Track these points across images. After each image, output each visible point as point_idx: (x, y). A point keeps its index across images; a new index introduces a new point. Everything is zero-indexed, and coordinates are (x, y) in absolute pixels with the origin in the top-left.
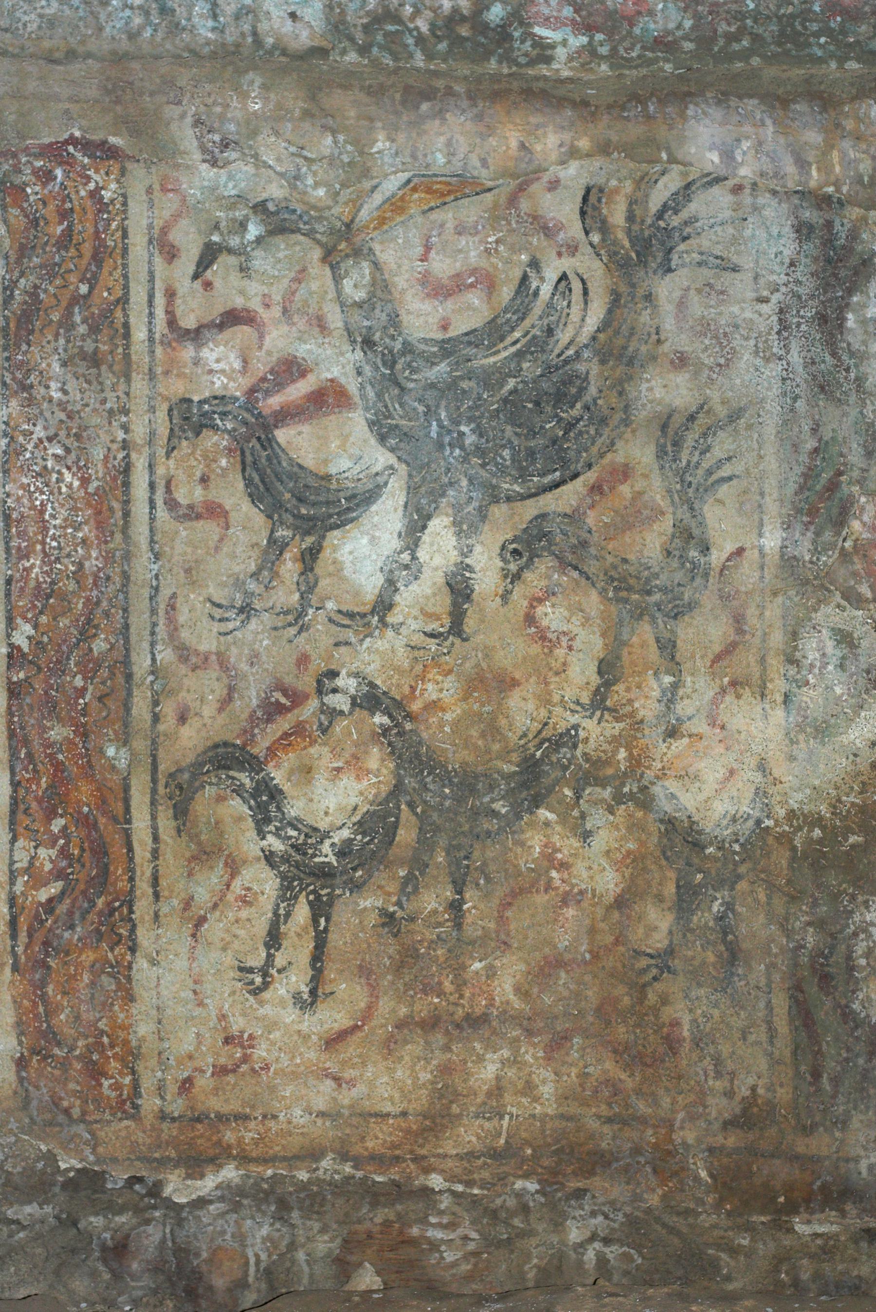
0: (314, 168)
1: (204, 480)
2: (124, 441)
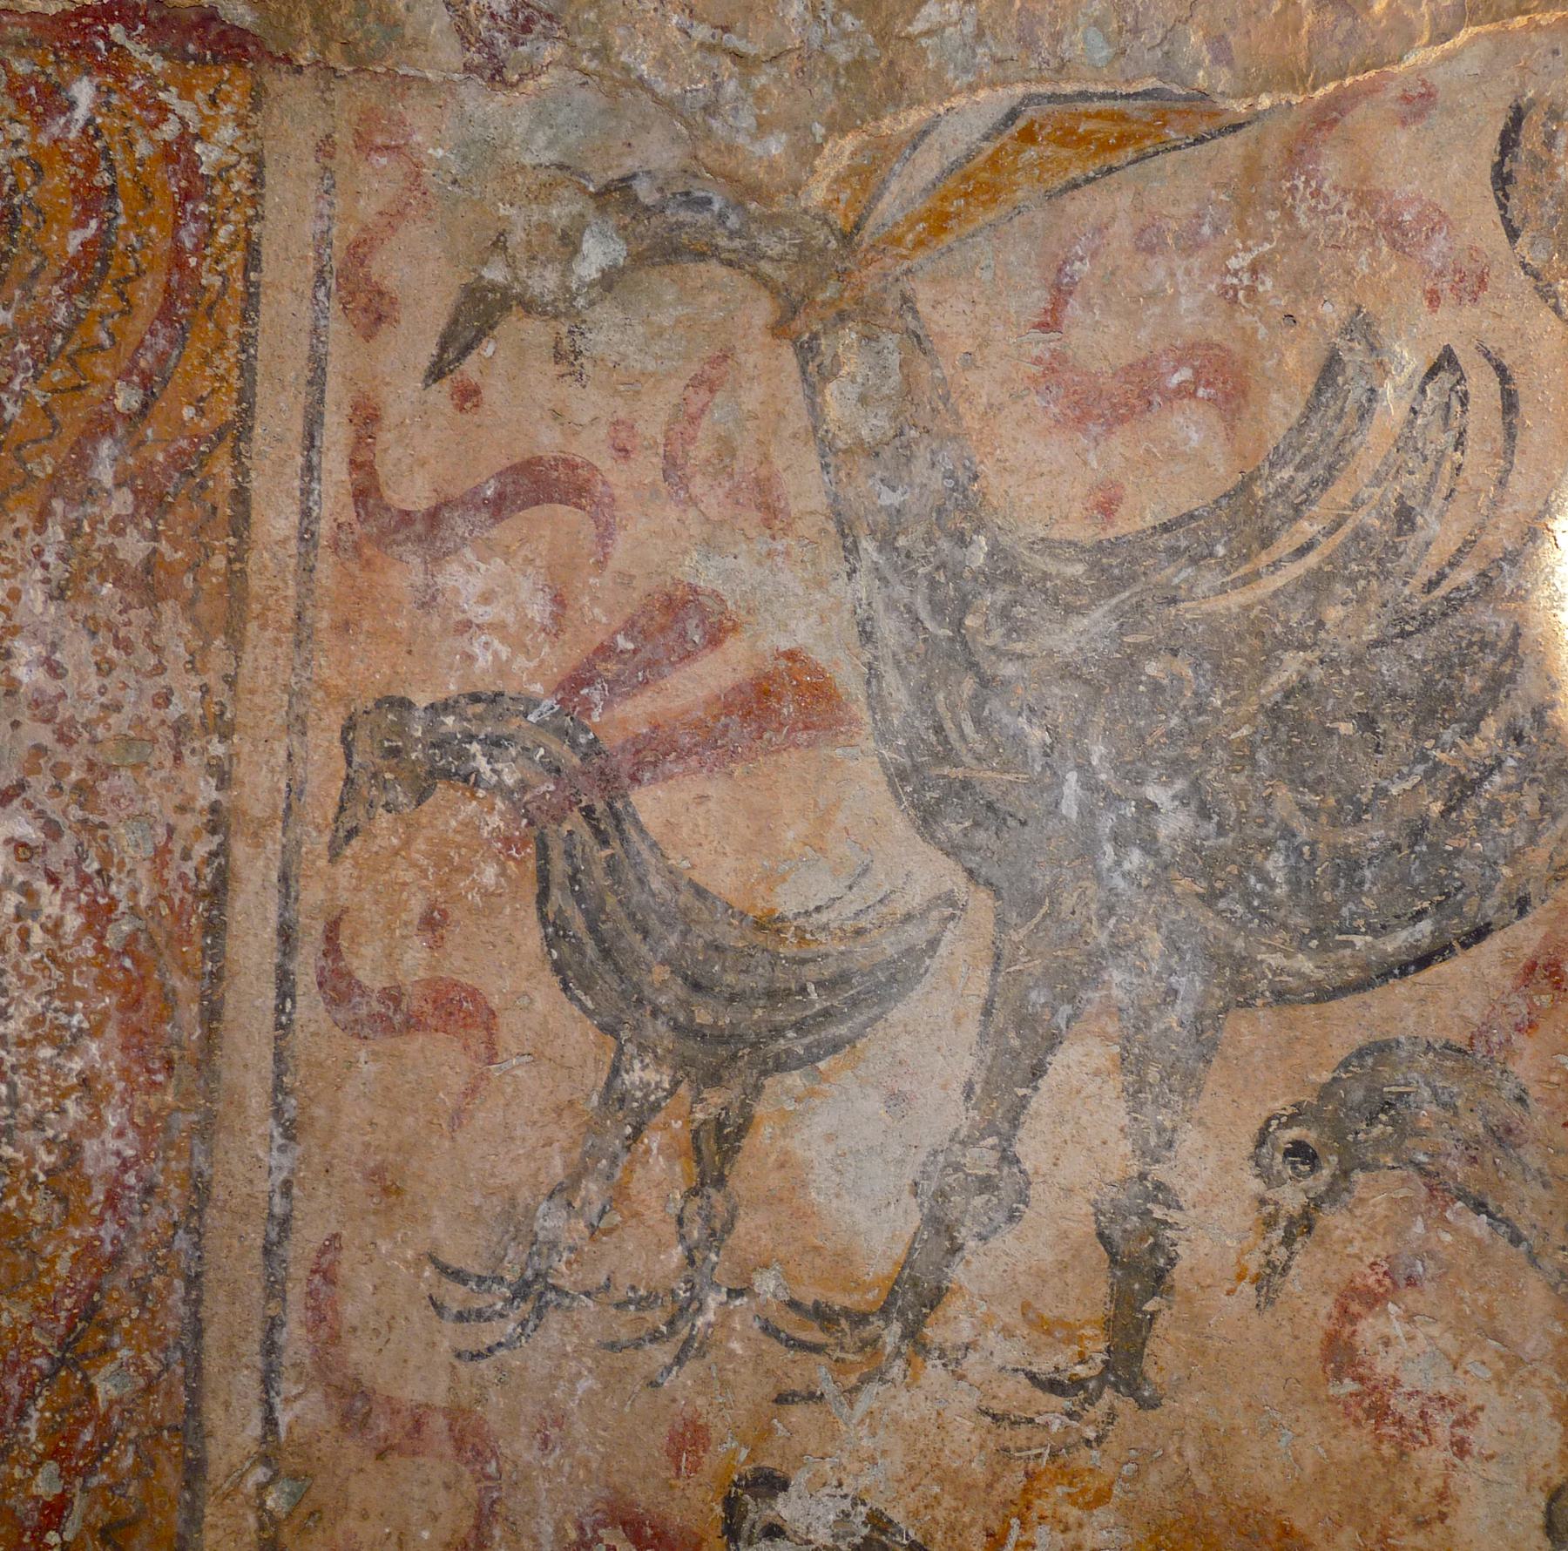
0: (760, 81)
1: (432, 923)
2: (214, 808)
